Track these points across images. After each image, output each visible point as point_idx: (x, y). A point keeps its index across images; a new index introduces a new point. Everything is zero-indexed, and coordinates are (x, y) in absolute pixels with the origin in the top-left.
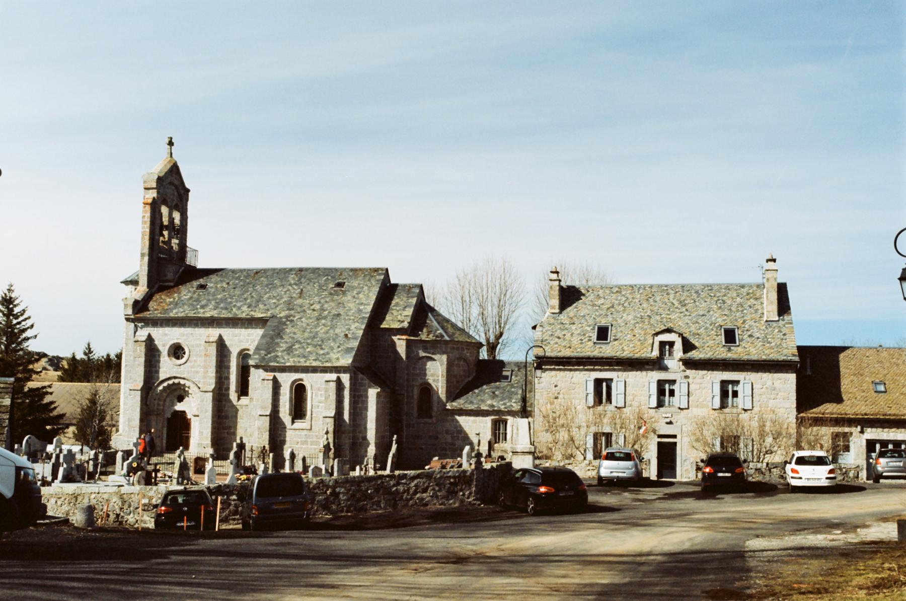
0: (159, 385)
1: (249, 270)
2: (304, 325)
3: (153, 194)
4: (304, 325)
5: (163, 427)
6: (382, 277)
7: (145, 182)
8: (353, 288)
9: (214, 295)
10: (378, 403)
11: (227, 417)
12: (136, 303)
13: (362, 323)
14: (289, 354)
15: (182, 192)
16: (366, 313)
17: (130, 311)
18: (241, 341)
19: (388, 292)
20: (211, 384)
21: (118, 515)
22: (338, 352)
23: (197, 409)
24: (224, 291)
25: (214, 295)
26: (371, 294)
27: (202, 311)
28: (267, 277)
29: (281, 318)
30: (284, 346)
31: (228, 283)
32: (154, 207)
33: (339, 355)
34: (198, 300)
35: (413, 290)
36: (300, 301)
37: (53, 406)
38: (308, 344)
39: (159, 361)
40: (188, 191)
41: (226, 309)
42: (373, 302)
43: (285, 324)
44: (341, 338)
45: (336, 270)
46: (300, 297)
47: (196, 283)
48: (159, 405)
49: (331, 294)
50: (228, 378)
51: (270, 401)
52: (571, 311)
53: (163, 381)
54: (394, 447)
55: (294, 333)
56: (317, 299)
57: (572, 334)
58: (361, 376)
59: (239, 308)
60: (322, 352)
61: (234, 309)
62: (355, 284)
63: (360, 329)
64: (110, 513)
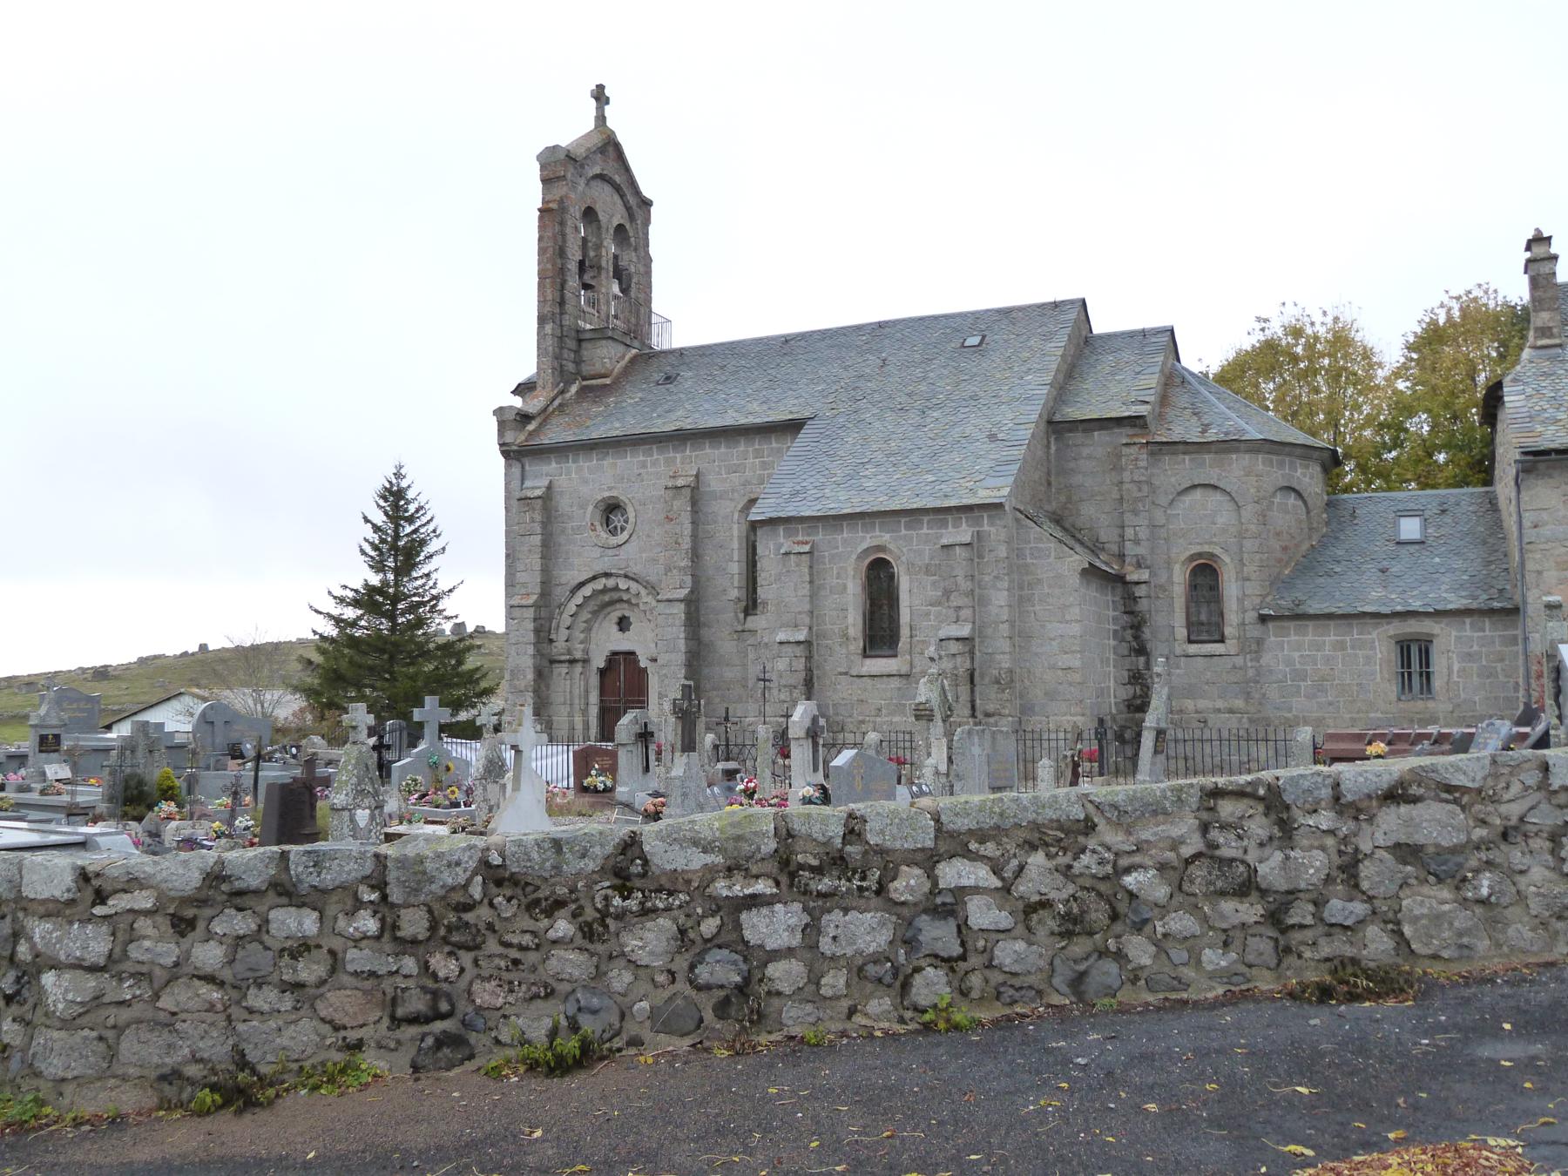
15: (632, 200)
40: (647, 204)
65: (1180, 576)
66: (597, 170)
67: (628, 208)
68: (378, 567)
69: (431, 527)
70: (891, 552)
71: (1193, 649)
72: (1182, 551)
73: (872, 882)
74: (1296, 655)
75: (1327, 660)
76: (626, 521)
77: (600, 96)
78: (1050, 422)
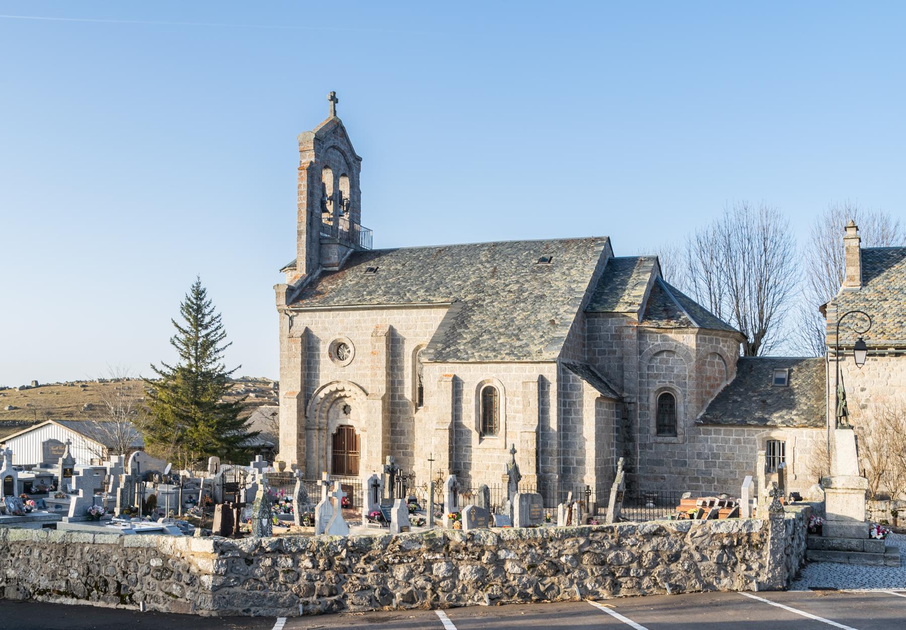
0: (319, 391)
1: (430, 248)
2: (496, 310)
3: (310, 157)
4: (496, 310)
5: (327, 445)
6: (602, 248)
7: (300, 144)
8: (563, 263)
9: (386, 278)
10: (597, 413)
11: (402, 433)
12: (290, 290)
13: (575, 305)
14: (474, 347)
15: (351, 159)
16: (579, 293)
17: (283, 301)
18: (417, 335)
19: (612, 271)
20: (380, 387)
21: (119, 585)
22: (542, 343)
23: (366, 420)
24: (397, 273)
25: (386, 278)
26: (586, 269)
27: (369, 297)
28: (452, 255)
29: (466, 302)
30: (468, 337)
31: (404, 265)
32: (313, 174)
33: (542, 346)
34: (365, 286)
35: (646, 264)
36: (492, 282)
37: (246, 423)
38: (500, 334)
39: (318, 362)
40: (359, 159)
41: (399, 294)
42: (589, 279)
43: (471, 310)
44: (545, 325)
45: (541, 242)
46: (492, 277)
47: (364, 266)
48: (320, 417)
49: (533, 271)
50: (401, 383)
51: (449, 410)
52: (879, 282)
53: (324, 387)
54: (620, 474)
55: (483, 321)
56: (514, 278)
57: (884, 315)
58: (572, 375)
59: (415, 292)
60: (518, 343)
61: (408, 295)
62: (566, 257)
63: (572, 313)
64: (109, 579)
65: (653, 401)
66: (331, 143)
67: (348, 164)
68: (186, 356)
69: (220, 332)
70: (488, 381)
71: (659, 439)
72: (657, 385)
73: (476, 556)
74: (714, 445)
75: (731, 449)
76: (349, 352)
77: (334, 99)
78: (585, 312)
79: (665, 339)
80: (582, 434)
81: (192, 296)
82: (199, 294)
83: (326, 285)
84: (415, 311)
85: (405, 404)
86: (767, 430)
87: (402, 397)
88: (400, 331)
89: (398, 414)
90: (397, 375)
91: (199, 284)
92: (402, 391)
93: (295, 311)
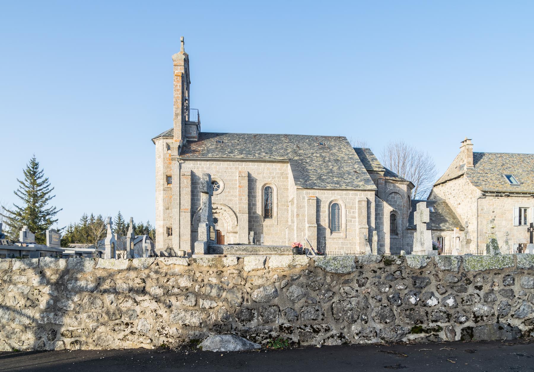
18: (264, 178)
70: (336, 200)
79: (394, 187)
80: (383, 230)
81: (31, 166)
82: (35, 165)
83: (194, 147)
84: (263, 164)
85: (257, 217)
86: (439, 232)
87: (255, 213)
88: (254, 175)
89: (253, 223)
90: (252, 200)
91: (34, 159)
92: (255, 209)
93: (182, 159)
